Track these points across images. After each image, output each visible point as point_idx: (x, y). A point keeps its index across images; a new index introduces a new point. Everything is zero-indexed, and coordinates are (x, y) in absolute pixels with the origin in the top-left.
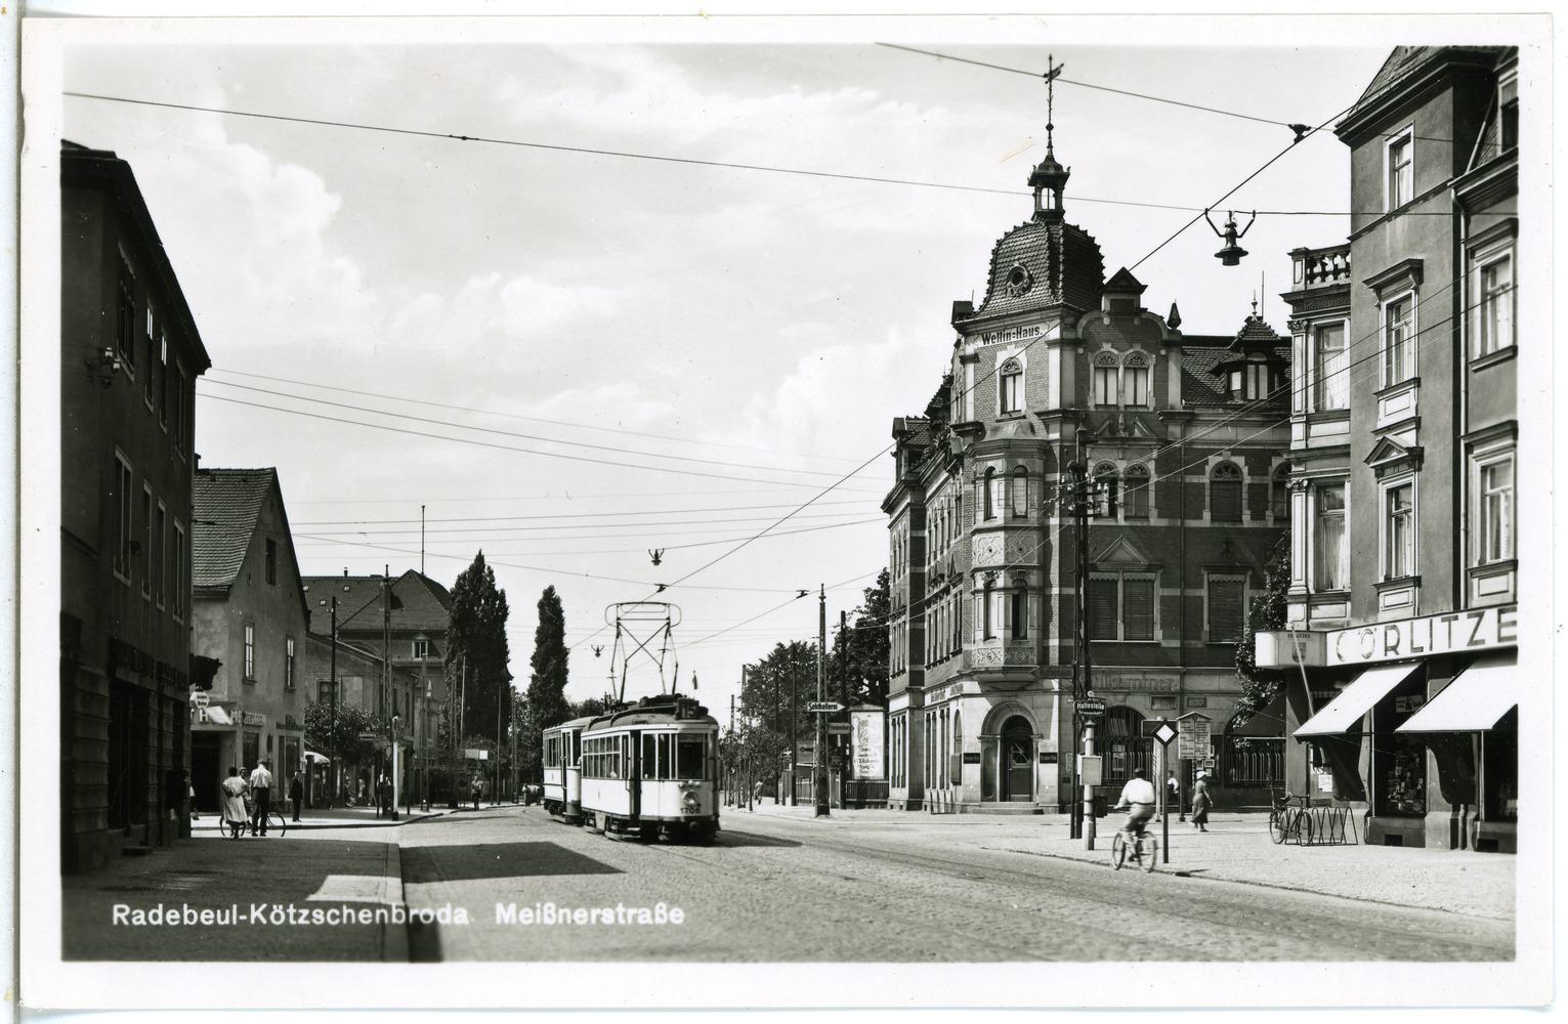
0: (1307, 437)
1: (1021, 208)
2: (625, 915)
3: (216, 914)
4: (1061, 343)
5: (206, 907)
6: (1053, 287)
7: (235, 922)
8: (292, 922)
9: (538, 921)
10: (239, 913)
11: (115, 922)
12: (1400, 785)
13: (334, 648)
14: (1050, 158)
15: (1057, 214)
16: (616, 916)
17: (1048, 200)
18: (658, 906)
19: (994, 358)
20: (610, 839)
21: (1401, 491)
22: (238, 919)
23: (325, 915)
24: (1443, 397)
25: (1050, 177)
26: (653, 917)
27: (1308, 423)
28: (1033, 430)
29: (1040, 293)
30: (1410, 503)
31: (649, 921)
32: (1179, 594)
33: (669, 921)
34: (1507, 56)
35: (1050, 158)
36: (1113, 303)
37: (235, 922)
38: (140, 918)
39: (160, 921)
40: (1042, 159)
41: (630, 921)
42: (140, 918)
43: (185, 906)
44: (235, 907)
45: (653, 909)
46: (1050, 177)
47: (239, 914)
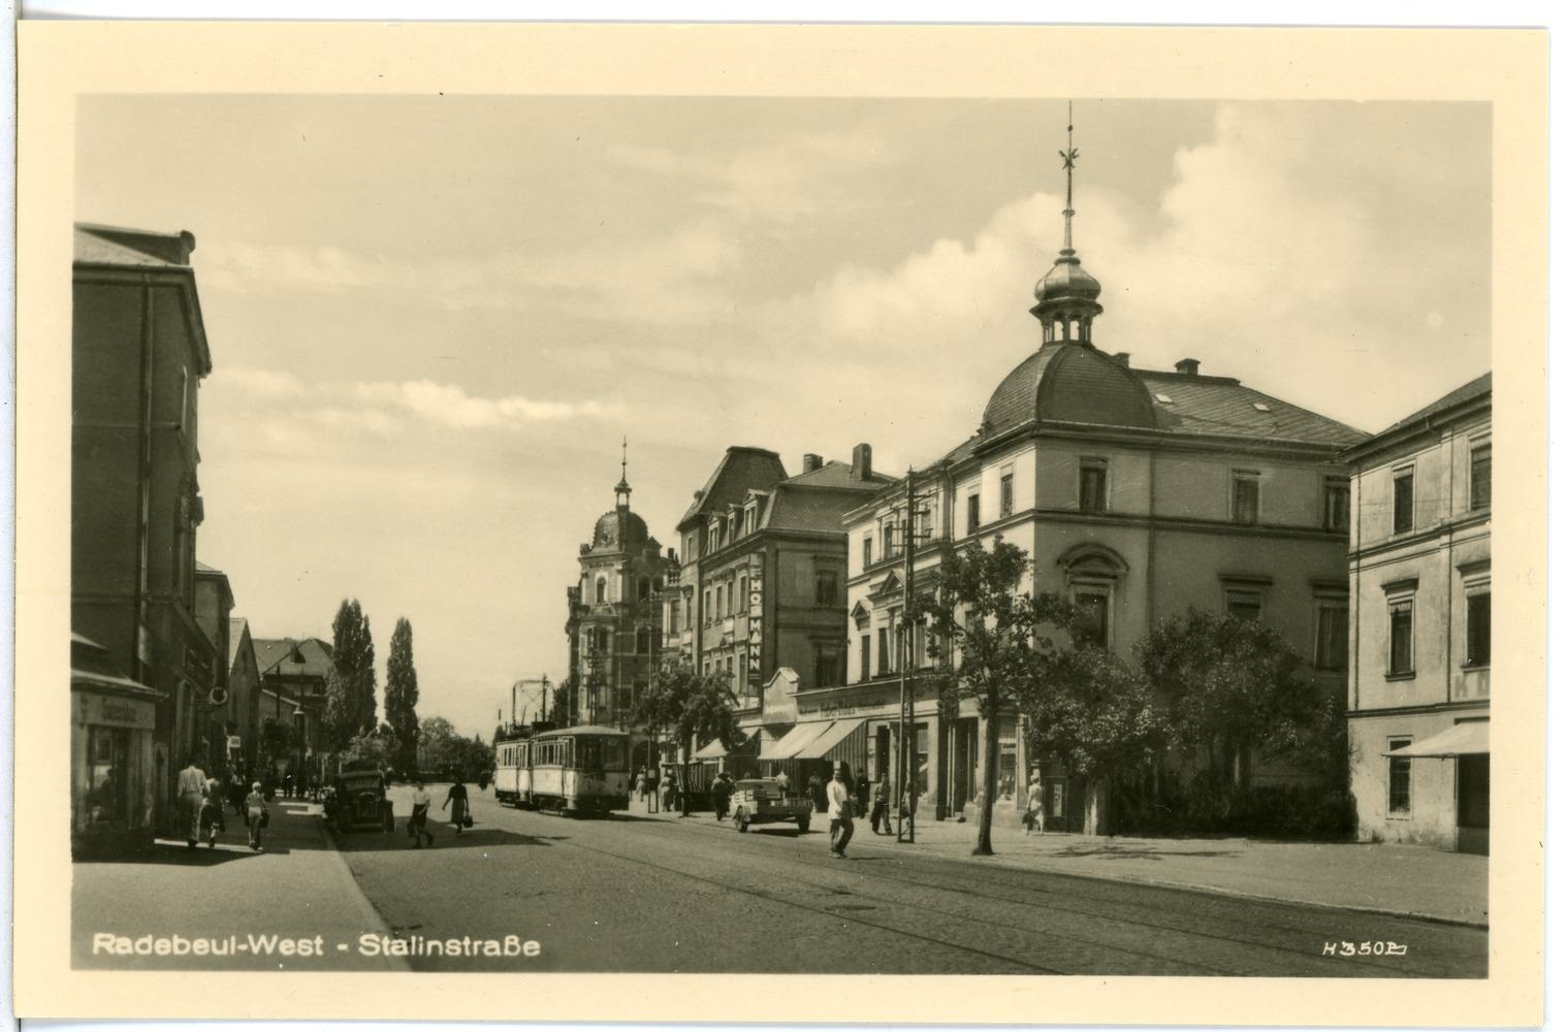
0: (668, 643)
1: (609, 503)
2: (471, 947)
3: (444, 951)
5: (451, 937)
8: (387, 953)
9: (413, 952)
10: (238, 943)
11: (96, 951)
13: (278, 707)
15: (626, 507)
16: (463, 947)
17: (623, 499)
18: (507, 939)
19: (594, 575)
22: (237, 950)
23: (133, 945)
24: (331, 699)
25: (623, 488)
26: (502, 947)
27: (668, 638)
28: (610, 612)
31: (498, 953)
33: (522, 953)
34: (1198, 363)
36: (647, 552)
41: (476, 952)
46: (623, 488)
47: (237, 943)
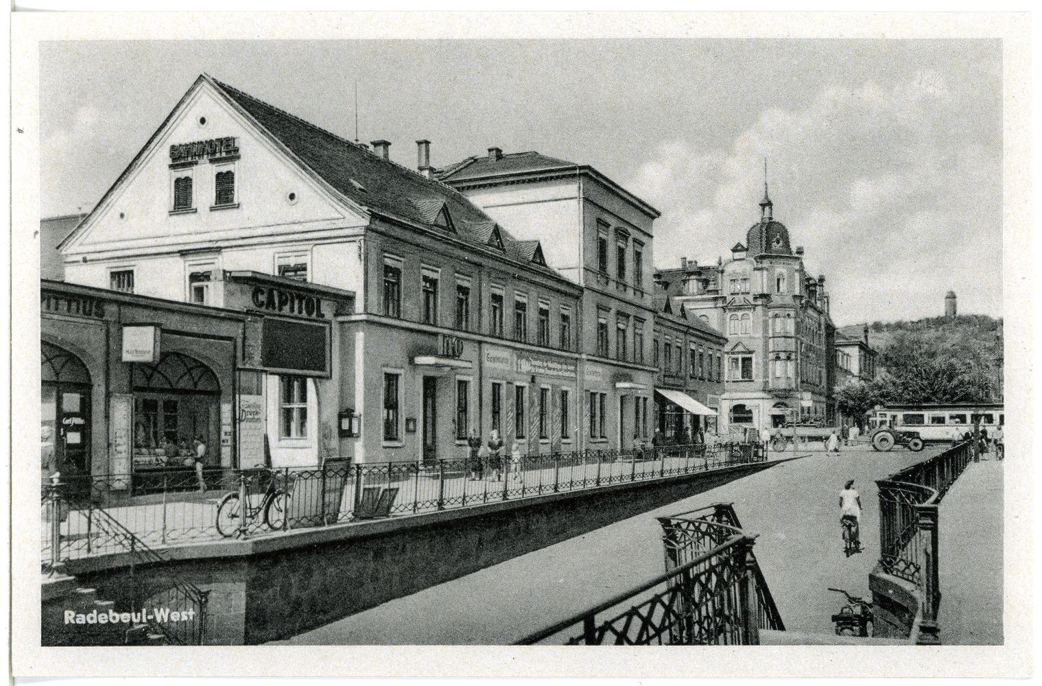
25: (767, 204)
38: (82, 619)
39: (95, 621)
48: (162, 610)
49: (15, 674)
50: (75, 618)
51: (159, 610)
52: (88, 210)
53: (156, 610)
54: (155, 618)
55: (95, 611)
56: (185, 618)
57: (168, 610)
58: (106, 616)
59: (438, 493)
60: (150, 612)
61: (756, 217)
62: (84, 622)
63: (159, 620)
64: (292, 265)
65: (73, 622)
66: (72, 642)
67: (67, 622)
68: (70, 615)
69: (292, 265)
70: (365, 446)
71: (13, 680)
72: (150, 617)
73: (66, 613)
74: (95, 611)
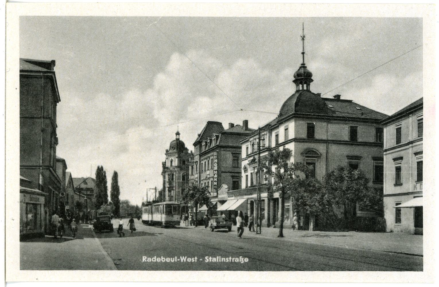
4: (178, 157)
6: (177, 150)
7: (176, 261)
10: (177, 258)
12: (293, 248)
14: (303, 66)
20: (216, 231)
21: (79, 164)
25: (178, 134)
29: (175, 151)
30: (214, 188)
32: (302, 217)
35: (303, 66)
37: (176, 261)
38: (150, 260)
39: (155, 261)
40: (299, 65)
42: (150, 260)
43: (162, 257)
44: (176, 257)
45: (239, 258)
48: (183, 257)
49: (6, 281)
50: (146, 259)
51: (182, 258)
52: (301, 62)
53: (181, 257)
54: (180, 260)
55: (155, 257)
56: (193, 261)
57: (186, 257)
58: (190, 259)
59: (153, 217)
60: (179, 258)
61: (174, 137)
62: (150, 261)
63: (182, 261)
64: (57, 137)
65: (146, 261)
66: (209, 269)
67: (143, 261)
68: (145, 258)
69: (57, 137)
70: (108, 200)
71: (6, 283)
72: (179, 260)
73: (143, 257)
74: (155, 257)
